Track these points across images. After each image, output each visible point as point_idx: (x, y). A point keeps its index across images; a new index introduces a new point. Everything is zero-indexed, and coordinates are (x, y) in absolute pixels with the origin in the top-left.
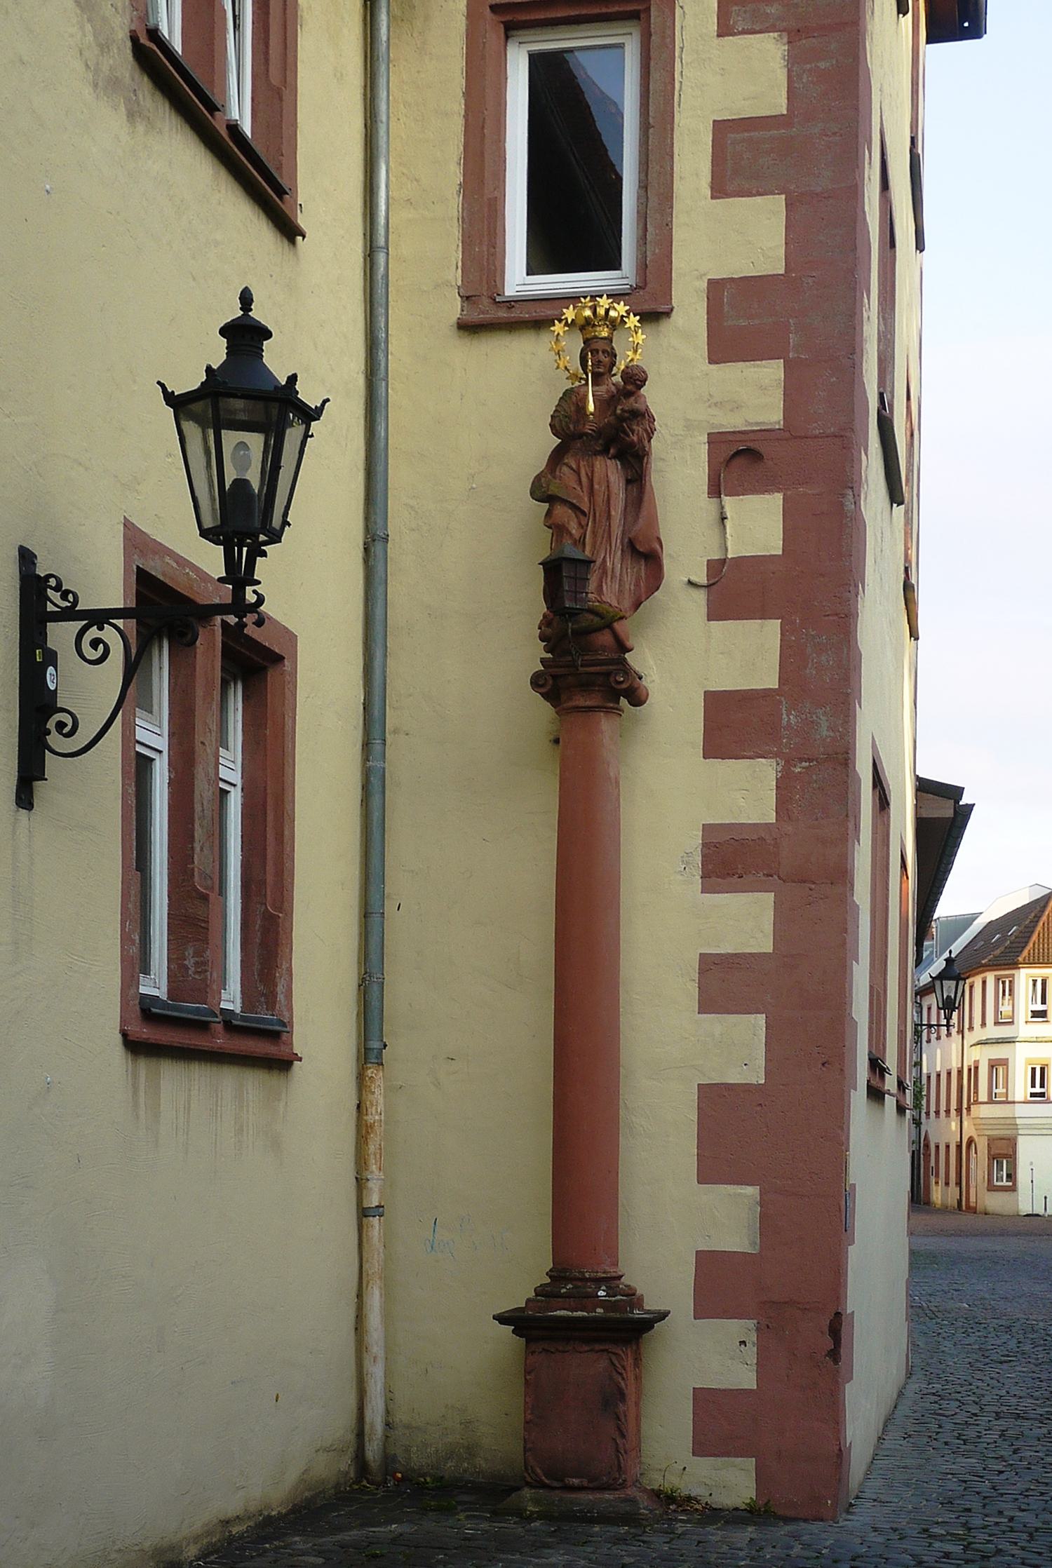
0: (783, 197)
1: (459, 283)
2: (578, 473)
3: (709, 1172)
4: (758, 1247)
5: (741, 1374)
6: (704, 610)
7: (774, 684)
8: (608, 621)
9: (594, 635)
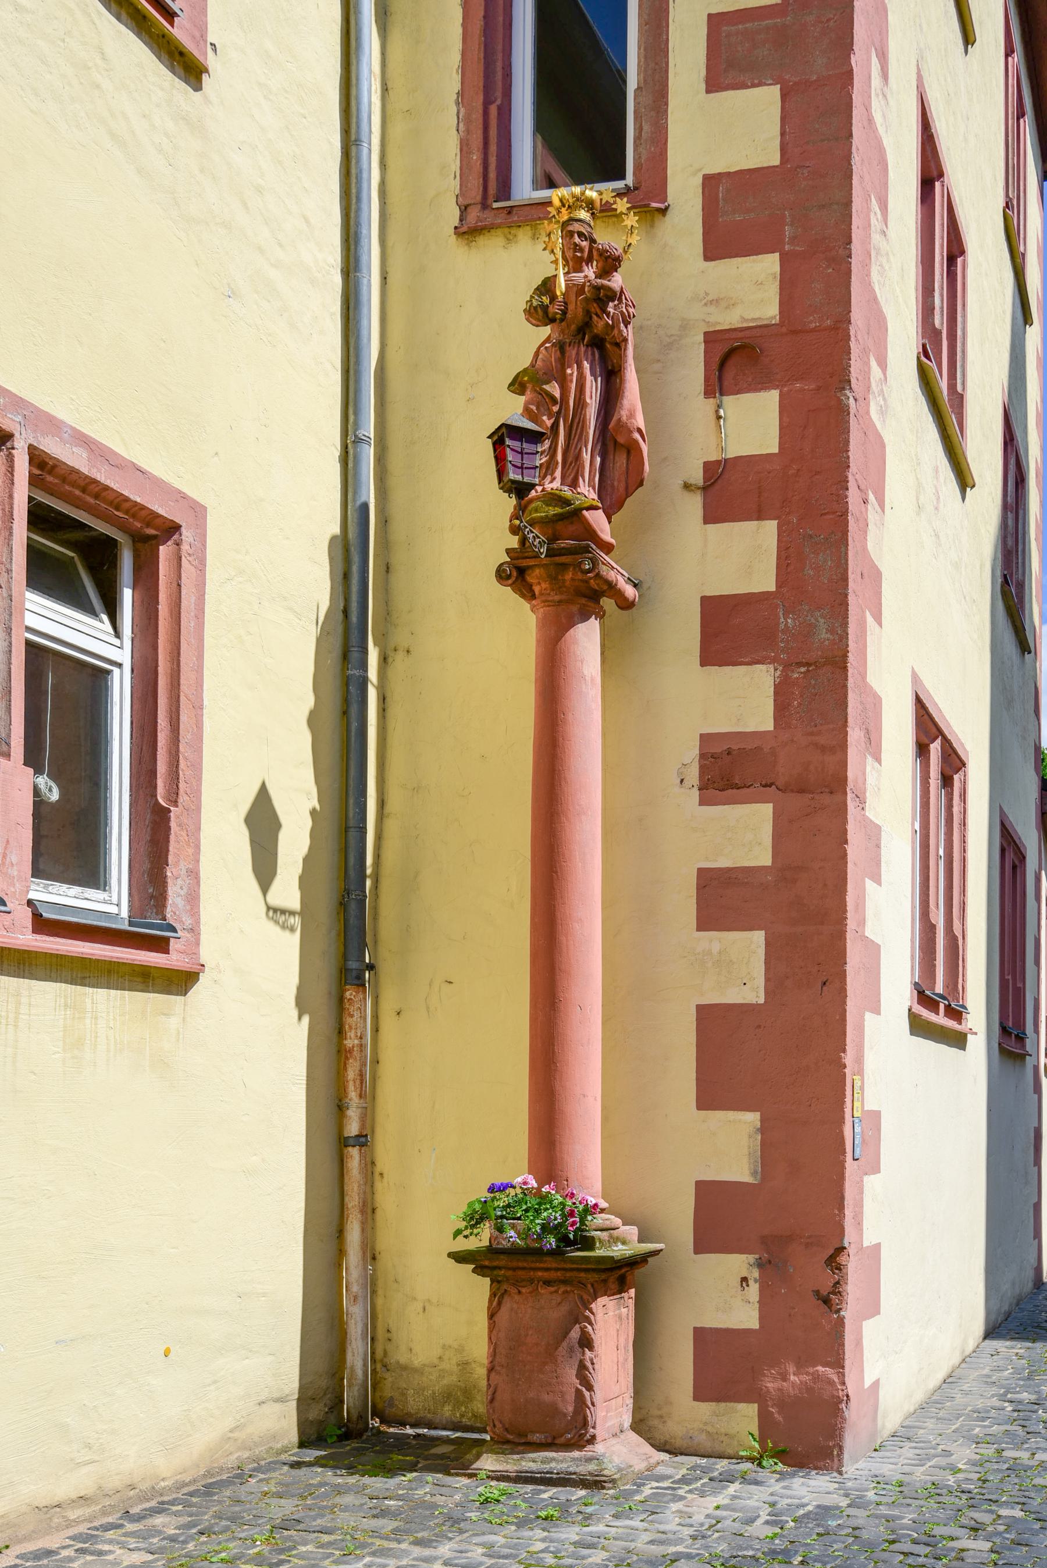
0: (778, 86)
3: (709, 1097)
4: (759, 1177)
5: (743, 1314)
7: (772, 588)
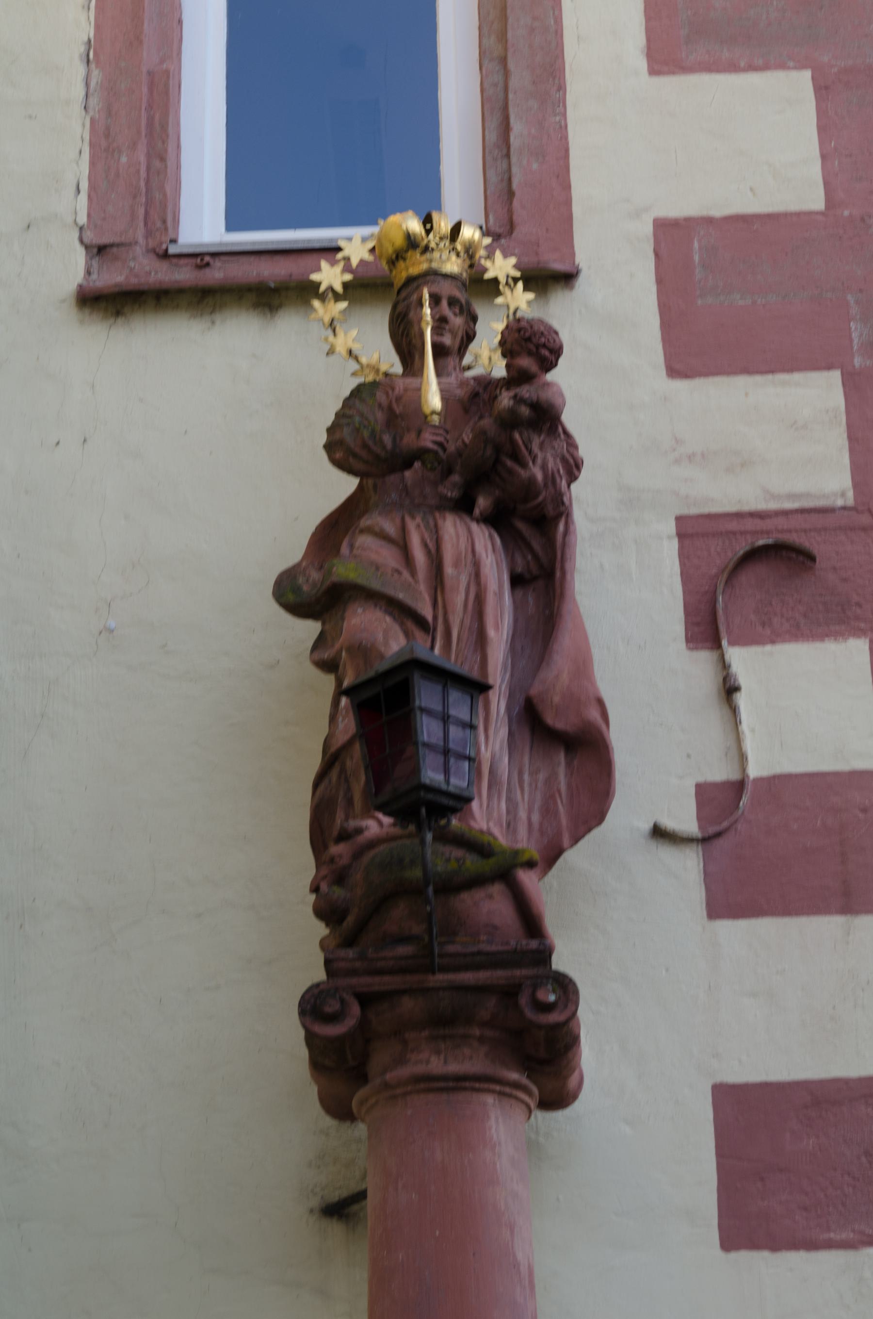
1: (83, 219)
2: (404, 548)
6: (697, 894)
8: (503, 871)
9: (465, 896)
